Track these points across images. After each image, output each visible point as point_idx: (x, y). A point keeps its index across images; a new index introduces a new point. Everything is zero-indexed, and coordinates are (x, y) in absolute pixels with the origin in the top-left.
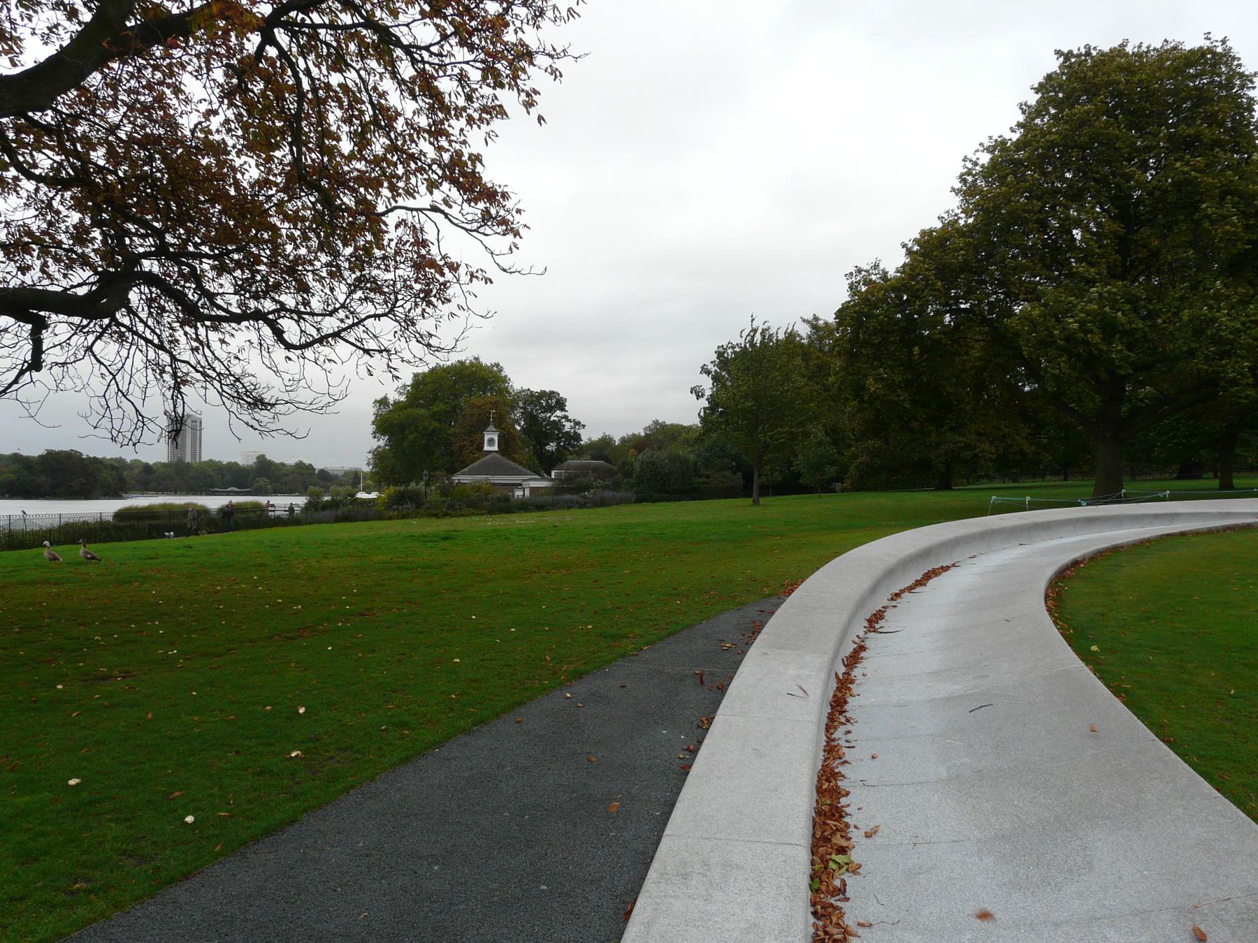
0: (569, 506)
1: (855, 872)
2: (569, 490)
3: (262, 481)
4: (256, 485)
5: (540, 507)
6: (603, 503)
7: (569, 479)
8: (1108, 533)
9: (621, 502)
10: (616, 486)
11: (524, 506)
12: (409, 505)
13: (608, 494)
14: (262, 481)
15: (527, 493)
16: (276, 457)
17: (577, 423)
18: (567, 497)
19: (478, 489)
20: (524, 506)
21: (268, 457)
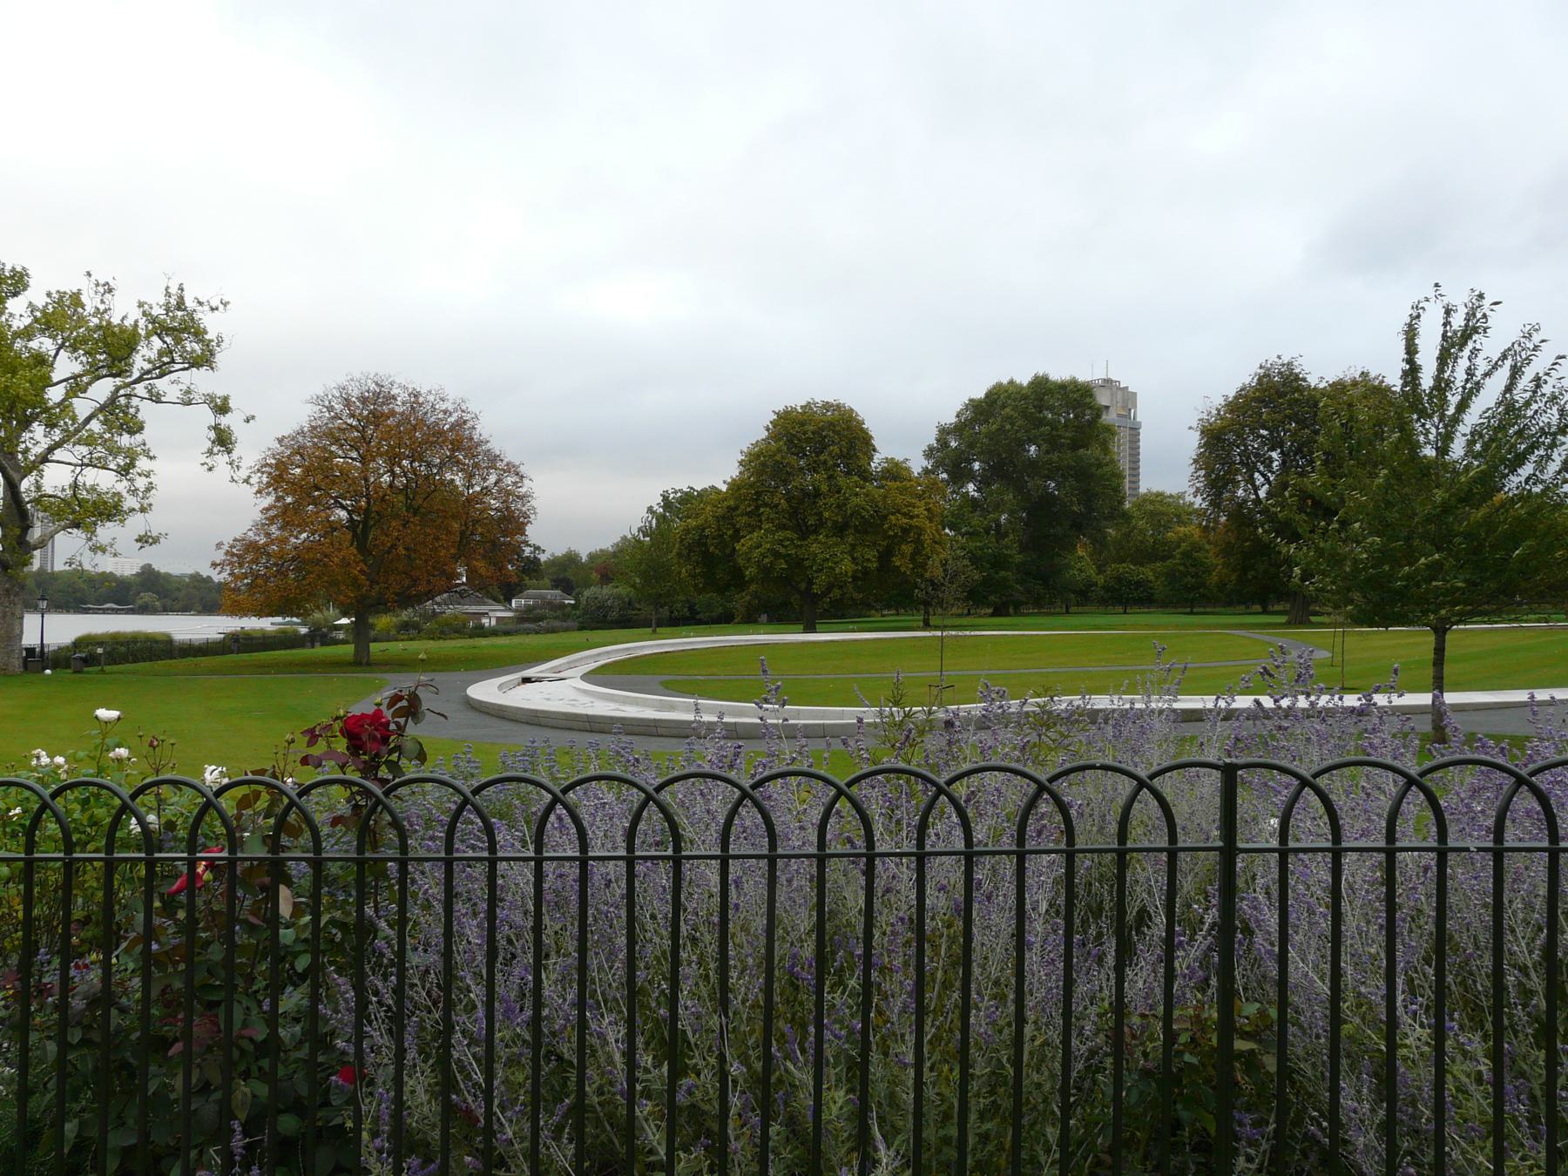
0: (528, 632)
1: (1481, 296)
2: (527, 620)
3: (146, 597)
4: (140, 602)
5: (507, 633)
6: (553, 631)
7: (529, 609)
8: (824, 715)
9: (567, 630)
10: (565, 617)
11: (493, 633)
12: (413, 632)
13: (557, 623)
14: (146, 597)
15: (493, 622)
16: (162, 566)
17: (537, 548)
18: (527, 625)
19: (1514, 726)
20: (493, 633)
21: (156, 567)
